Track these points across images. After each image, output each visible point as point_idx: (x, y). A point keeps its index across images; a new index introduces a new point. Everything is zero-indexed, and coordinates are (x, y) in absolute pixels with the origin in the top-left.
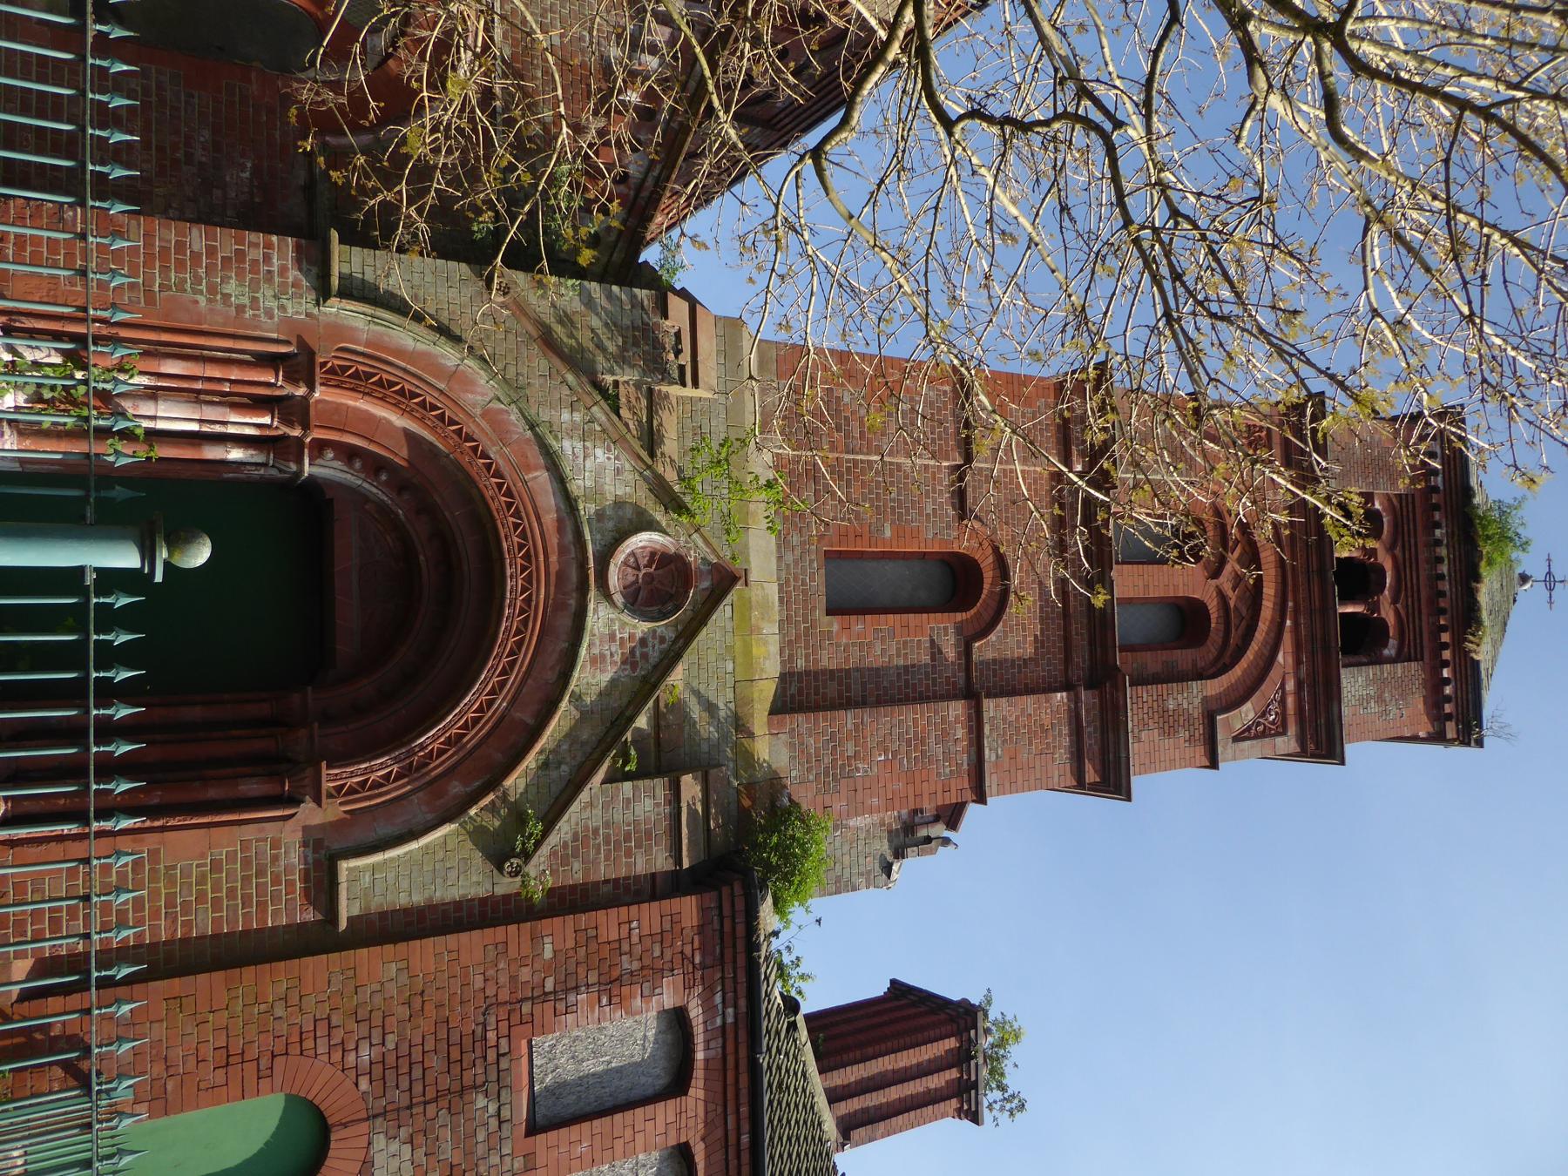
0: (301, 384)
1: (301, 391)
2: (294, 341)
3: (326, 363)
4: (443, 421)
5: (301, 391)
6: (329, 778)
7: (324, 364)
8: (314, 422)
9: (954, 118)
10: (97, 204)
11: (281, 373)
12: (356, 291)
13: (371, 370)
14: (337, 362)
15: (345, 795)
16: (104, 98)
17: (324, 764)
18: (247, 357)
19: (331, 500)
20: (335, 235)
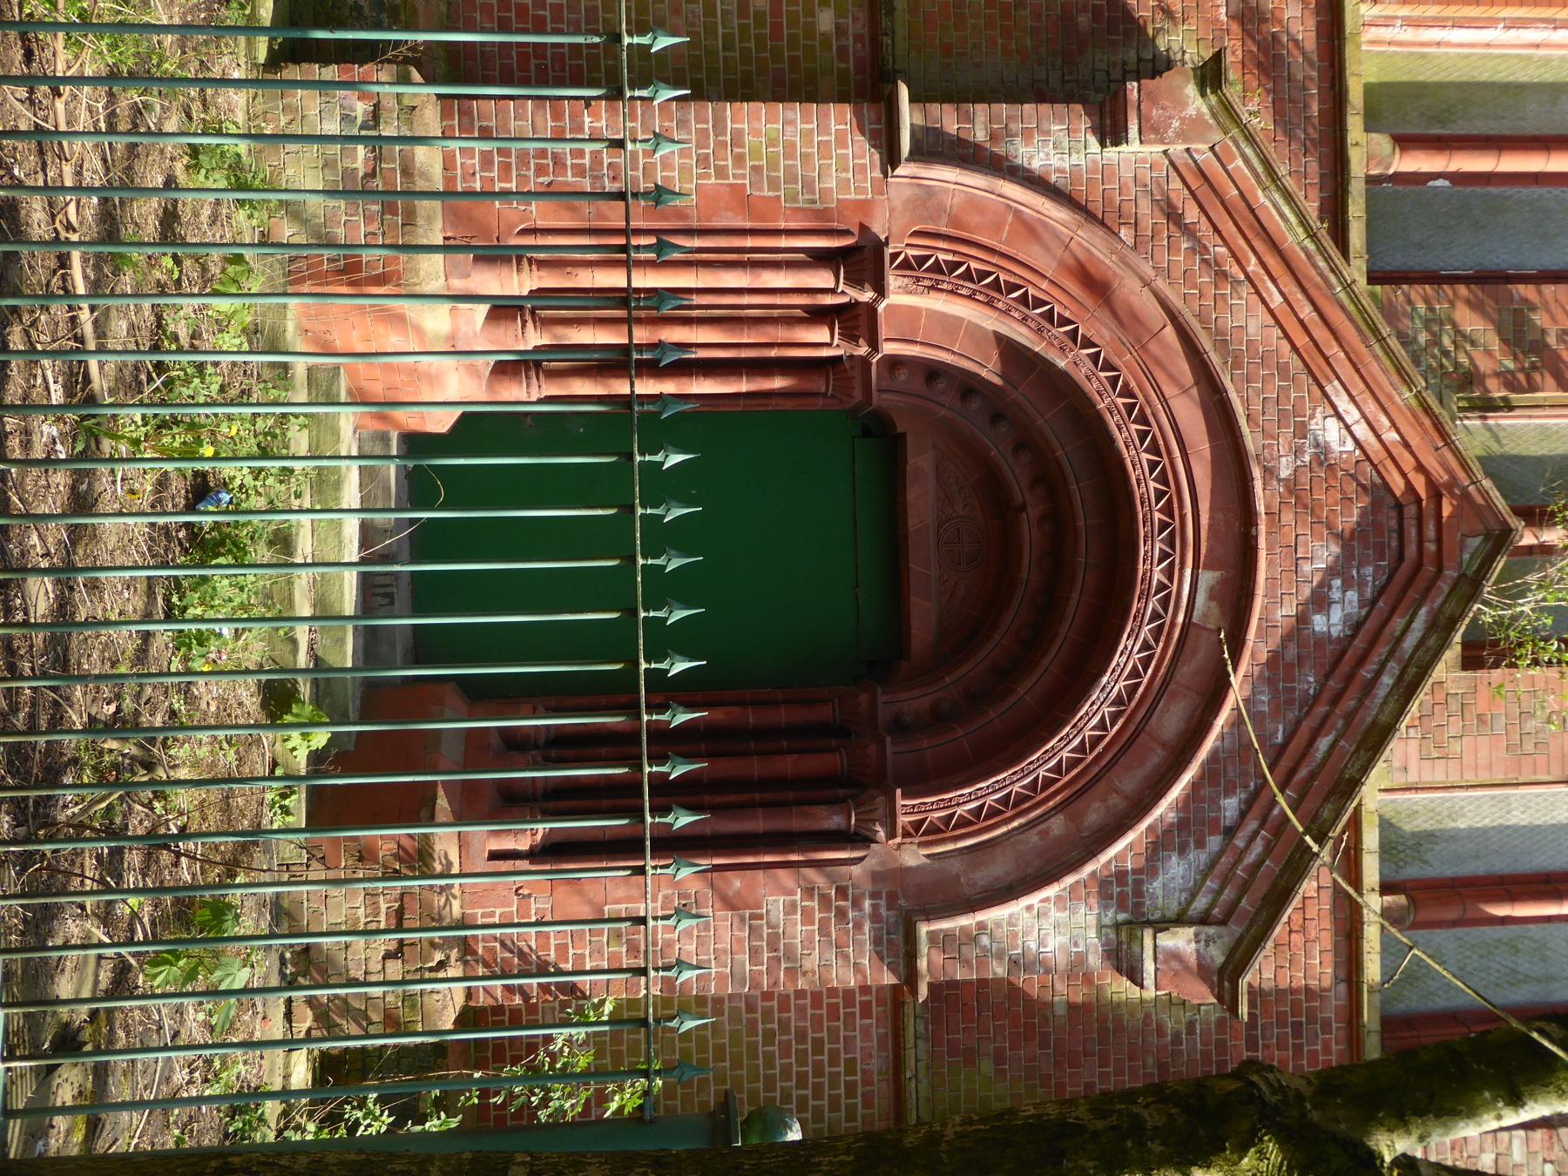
0: (867, 285)
1: (867, 296)
2: (855, 230)
3: (898, 254)
4: (1051, 321)
5: (867, 296)
6: (907, 808)
7: (895, 256)
8: (883, 332)
9: (1158, 935)
10: (637, 93)
11: (837, 331)
12: (933, 148)
13: (956, 259)
14: (912, 252)
15: (924, 834)
16: (645, 40)
17: (899, 792)
18: (798, 312)
19: (904, 434)
20: (904, 92)
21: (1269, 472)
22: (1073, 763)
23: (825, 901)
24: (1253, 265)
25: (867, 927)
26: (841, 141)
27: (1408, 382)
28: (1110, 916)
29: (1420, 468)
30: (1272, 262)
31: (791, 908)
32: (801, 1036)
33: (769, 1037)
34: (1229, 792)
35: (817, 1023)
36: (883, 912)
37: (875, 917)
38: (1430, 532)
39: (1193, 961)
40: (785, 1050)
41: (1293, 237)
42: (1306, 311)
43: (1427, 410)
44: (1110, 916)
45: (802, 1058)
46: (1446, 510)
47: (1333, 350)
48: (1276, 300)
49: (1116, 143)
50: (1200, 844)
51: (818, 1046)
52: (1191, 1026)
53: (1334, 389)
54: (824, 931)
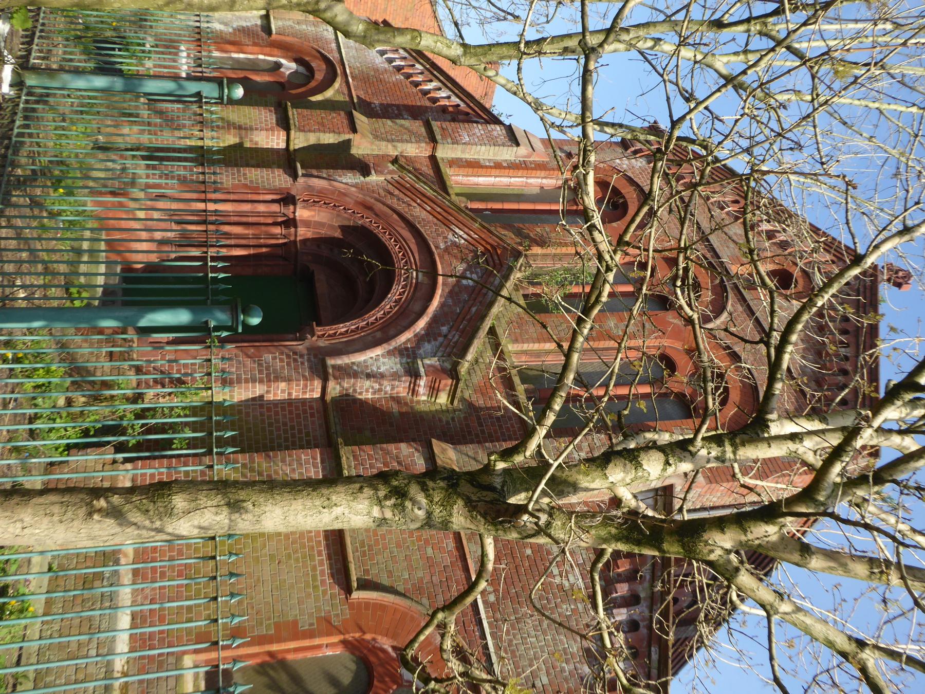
16: (221, 434)
20: (299, 165)
21: (437, 247)
22: (381, 318)
23: (288, 356)
24: (419, 201)
25: (306, 364)
26: (279, 176)
27: (476, 221)
28: (404, 360)
29: (488, 243)
30: (424, 199)
31: (274, 358)
32: (285, 424)
33: (270, 425)
34: (443, 325)
35: (291, 420)
36: (312, 359)
37: (309, 360)
38: (496, 258)
39: (439, 367)
40: (278, 429)
41: (429, 192)
42: (439, 209)
43: (484, 227)
44: (404, 360)
45: (286, 432)
46: (499, 252)
47: (450, 218)
48: (429, 208)
49: (368, 176)
50: (435, 339)
51: (293, 428)
52: (453, 419)
53: (453, 227)
54: (288, 364)
